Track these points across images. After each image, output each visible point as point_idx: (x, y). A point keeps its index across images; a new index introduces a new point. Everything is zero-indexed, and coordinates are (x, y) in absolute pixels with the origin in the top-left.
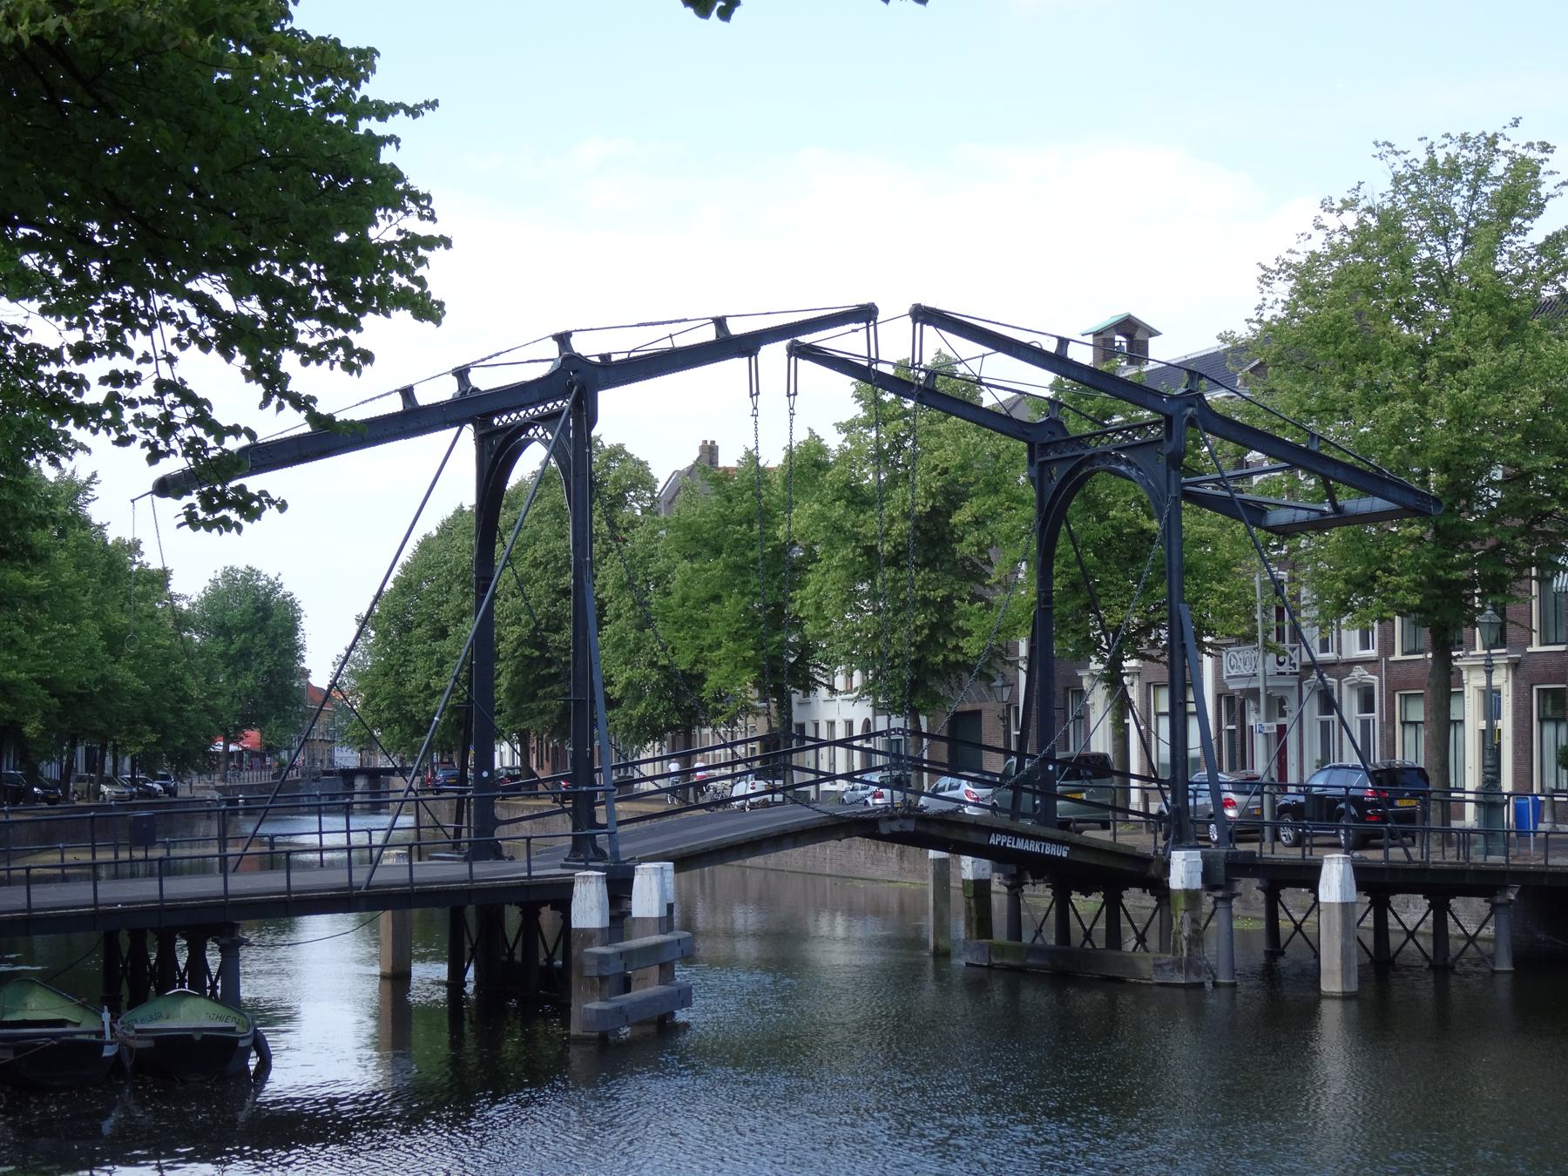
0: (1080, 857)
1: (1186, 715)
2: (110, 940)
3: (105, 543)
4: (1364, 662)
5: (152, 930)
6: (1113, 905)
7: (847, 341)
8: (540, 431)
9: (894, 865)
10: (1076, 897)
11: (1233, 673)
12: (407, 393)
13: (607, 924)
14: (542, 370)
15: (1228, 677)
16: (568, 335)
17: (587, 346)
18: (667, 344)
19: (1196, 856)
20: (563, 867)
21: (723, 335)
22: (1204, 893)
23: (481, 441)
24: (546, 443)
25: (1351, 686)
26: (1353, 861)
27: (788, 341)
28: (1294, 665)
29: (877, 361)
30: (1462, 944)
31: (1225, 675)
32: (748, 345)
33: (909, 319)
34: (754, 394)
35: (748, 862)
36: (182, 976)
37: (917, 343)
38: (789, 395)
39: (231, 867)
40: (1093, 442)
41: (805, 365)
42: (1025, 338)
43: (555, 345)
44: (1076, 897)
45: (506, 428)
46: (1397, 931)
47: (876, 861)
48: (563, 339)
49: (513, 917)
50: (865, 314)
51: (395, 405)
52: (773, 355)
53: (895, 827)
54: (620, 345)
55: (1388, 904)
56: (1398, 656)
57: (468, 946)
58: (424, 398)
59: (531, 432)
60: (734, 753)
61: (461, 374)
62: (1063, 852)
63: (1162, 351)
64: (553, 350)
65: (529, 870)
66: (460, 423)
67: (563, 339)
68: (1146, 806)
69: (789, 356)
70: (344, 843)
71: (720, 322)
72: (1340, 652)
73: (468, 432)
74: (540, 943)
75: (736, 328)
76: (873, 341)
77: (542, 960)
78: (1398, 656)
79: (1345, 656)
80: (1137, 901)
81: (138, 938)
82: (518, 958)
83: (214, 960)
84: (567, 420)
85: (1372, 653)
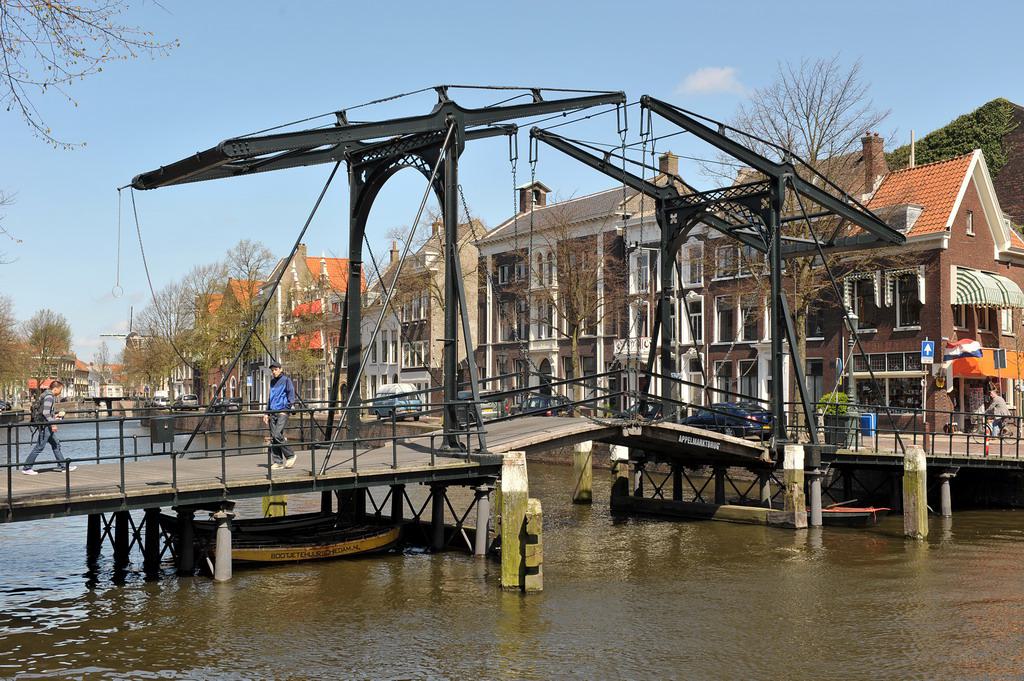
16: (446, 87)
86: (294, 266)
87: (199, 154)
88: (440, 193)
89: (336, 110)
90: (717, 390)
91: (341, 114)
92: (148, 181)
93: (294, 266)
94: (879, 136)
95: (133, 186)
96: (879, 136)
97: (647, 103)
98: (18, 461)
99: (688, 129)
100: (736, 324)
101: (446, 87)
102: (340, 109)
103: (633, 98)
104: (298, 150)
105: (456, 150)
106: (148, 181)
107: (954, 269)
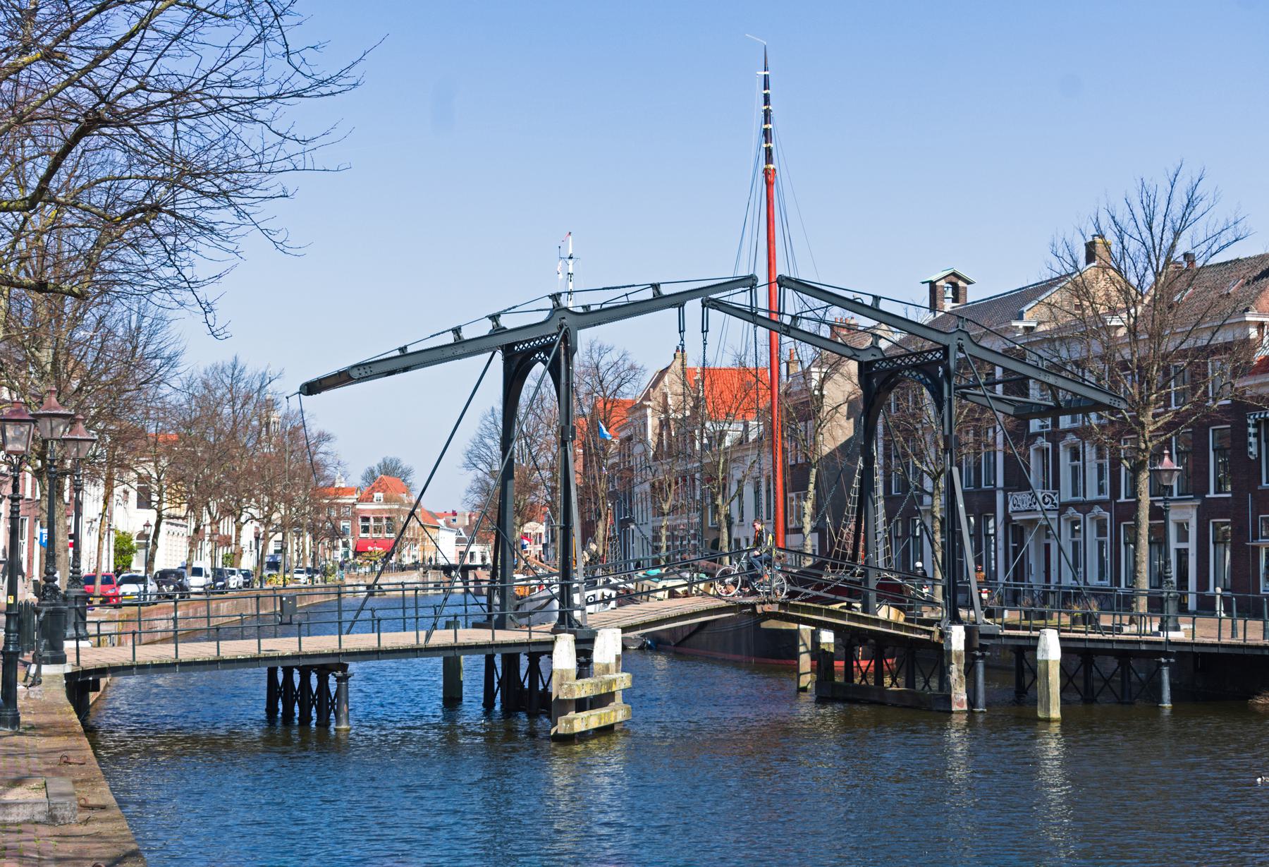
2: (272, 673)
5: (297, 667)
7: (740, 298)
8: (542, 355)
11: (1015, 508)
12: (456, 331)
14: (543, 316)
15: (1013, 512)
17: (573, 303)
19: (962, 628)
23: (507, 361)
24: (545, 363)
25: (1066, 520)
28: (1055, 504)
30: (1101, 684)
31: (1010, 510)
32: (677, 301)
34: (681, 331)
36: (314, 697)
38: (703, 332)
39: (344, 630)
41: (714, 314)
42: (849, 295)
43: (550, 301)
49: (524, 662)
51: (449, 338)
52: (694, 306)
54: (596, 300)
55: (1093, 662)
56: (1123, 499)
57: (496, 680)
58: (466, 334)
59: (537, 355)
63: (974, 295)
64: (549, 304)
65: (1245, 640)
68: (258, 611)
69: (703, 306)
70: (420, 610)
71: (655, 287)
72: (1085, 496)
73: (499, 356)
77: (541, 687)
78: (1123, 499)
79: (1088, 498)
81: (288, 672)
82: (526, 684)
84: (559, 348)
91: (456, 331)
104: (460, 348)
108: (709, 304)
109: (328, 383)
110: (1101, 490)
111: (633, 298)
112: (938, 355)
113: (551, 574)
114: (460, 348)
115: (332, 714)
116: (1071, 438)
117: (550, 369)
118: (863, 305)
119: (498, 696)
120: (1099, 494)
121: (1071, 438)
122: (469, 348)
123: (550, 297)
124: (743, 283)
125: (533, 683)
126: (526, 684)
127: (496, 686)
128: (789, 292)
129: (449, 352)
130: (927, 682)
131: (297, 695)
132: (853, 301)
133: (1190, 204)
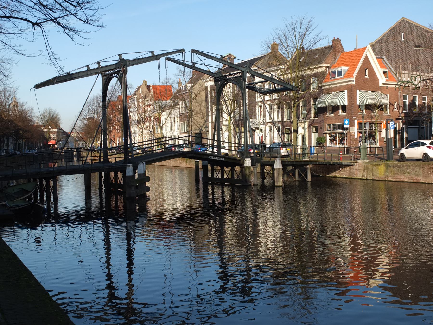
0: (226, 160)
1: (244, 132)
3: (46, 146)
4: (278, 122)
6: (233, 170)
7: (178, 57)
8: (115, 75)
9: (185, 164)
10: (225, 169)
12: (88, 66)
13: (407, 158)
16: (121, 54)
17: (125, 57)
18: (141, 57)
20: (123, 164)
21: (153, 55)
22: (251, 167)
24: (117, 77)
26: (281, 160)
27: (165, 57)
29: (185, 61)
33: (191, 52)
35: (156, 164)
36: (45, 188)
37: (192, 57)
40: (227, 77)
44: (225, 169)
45: (108, 74)
46: (350, 172)
47: (181, 163)
48: (120, 55)
50: (182, 51)
52: (162, 59)
53: (190, 155)
57: (103, 180)
58: (91, 67)
59: (114, 75)
60: (154, 141)
61: (98, 63)
62: (223, 159)
66: (98, 73)
67: (120, 55)
71: (152, 52)
74: (118, 180)
75: (156, 53)
76: (183, 57)
80: (237, 168)
82: (114, 182)
83: (51, 183)
85: (280, 120)
86: (141, 90)
87: (48, 80)
88: (121, 83)
89: (96, 61)
90: (209, 139)
91: (88, 66)
92: (38, 86)
93: (141, 90)
94: (339, 39)
95: (34, 87)
96: (339, 39)
97: (193, 51)
98: (135, 142)
99: (209, 58)
100: (356, 100)
101: (100, 62)
102: (87, 65)
103: (188, 50)
104: (89, 72)
105: (125, 72)
106: (38, 86)
107: (358, 91)
108: (168, 59)
109: (80, 75)
110: (278, 118)
111: (144, 56)
112: (241, 74)
113: (230, 150)
114: (89, 72)
115: (370, 276)
116: (269, 102)
117: (119, 80)
118: (217, 58)
119: (104, 186)
120: (278, 119)
121: (269, 102)
122: (92, 72)
123: (119, 55)
124: (180, 52)
125: (116, 181)
126: (114, 182)
127: (103, 182)
128: (195, 54)
129: (85, 74)
130: (217, 175)
131: (45, 189)
132: (215, 57)
133: (307, 30)
